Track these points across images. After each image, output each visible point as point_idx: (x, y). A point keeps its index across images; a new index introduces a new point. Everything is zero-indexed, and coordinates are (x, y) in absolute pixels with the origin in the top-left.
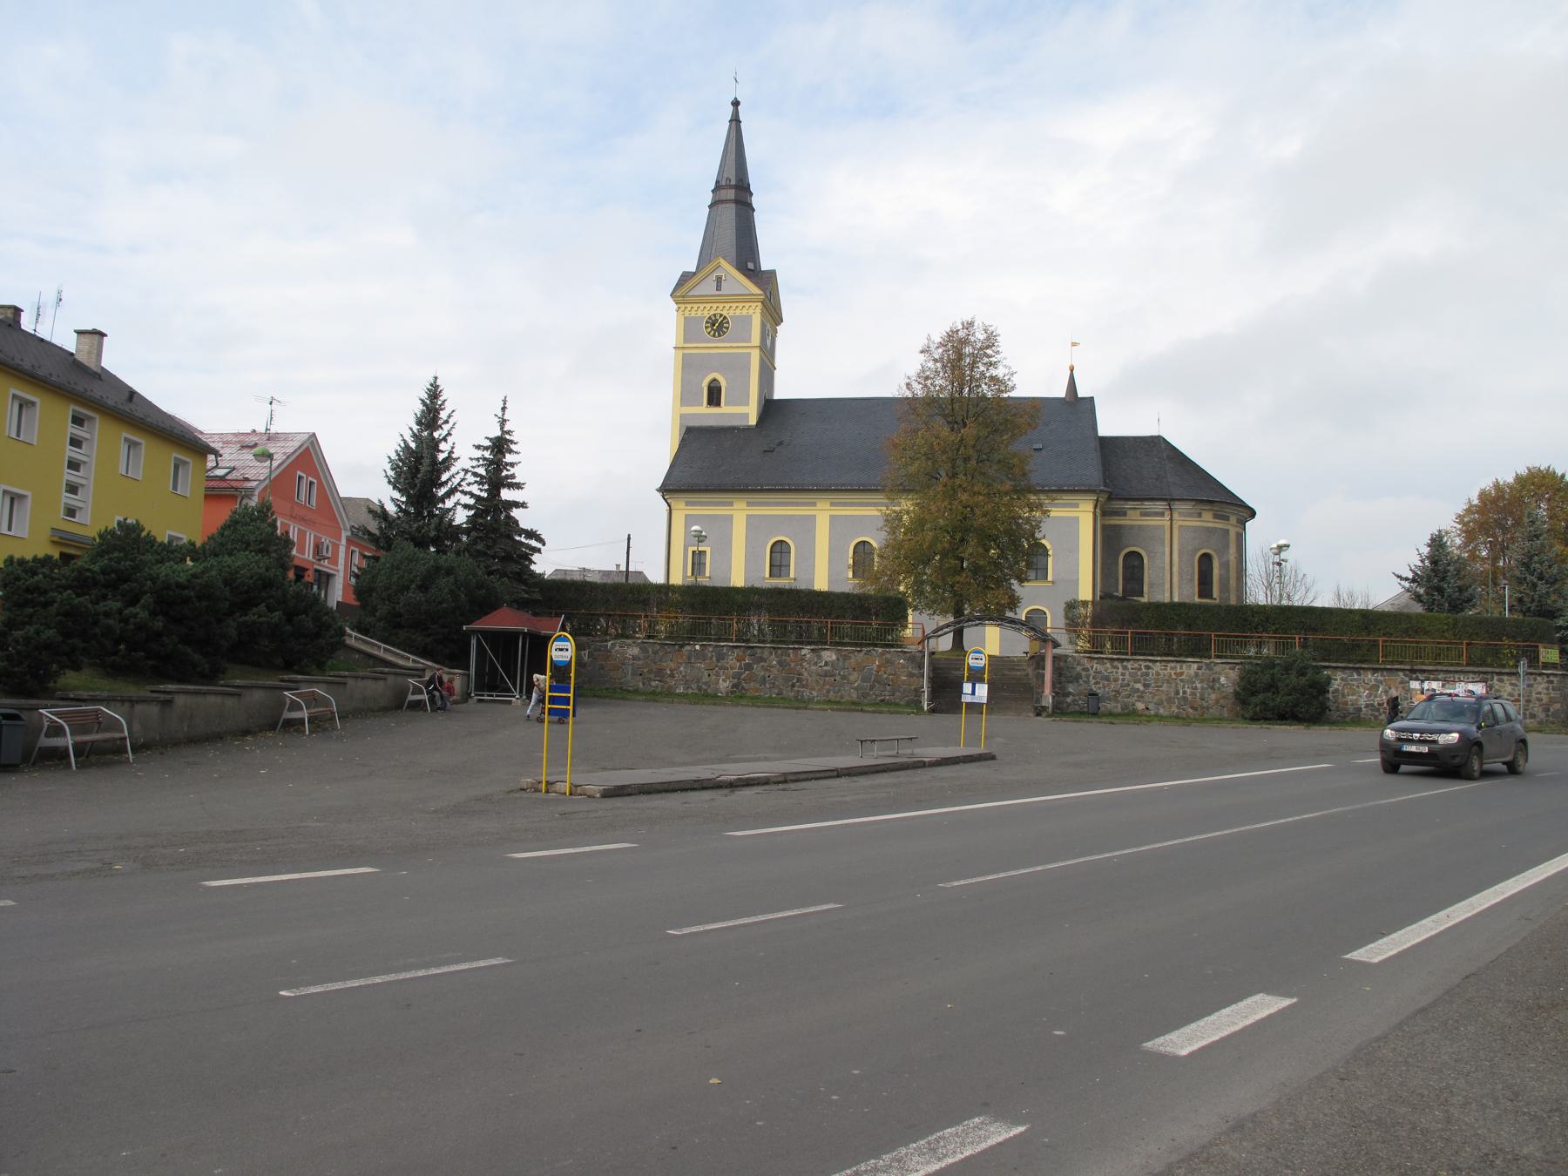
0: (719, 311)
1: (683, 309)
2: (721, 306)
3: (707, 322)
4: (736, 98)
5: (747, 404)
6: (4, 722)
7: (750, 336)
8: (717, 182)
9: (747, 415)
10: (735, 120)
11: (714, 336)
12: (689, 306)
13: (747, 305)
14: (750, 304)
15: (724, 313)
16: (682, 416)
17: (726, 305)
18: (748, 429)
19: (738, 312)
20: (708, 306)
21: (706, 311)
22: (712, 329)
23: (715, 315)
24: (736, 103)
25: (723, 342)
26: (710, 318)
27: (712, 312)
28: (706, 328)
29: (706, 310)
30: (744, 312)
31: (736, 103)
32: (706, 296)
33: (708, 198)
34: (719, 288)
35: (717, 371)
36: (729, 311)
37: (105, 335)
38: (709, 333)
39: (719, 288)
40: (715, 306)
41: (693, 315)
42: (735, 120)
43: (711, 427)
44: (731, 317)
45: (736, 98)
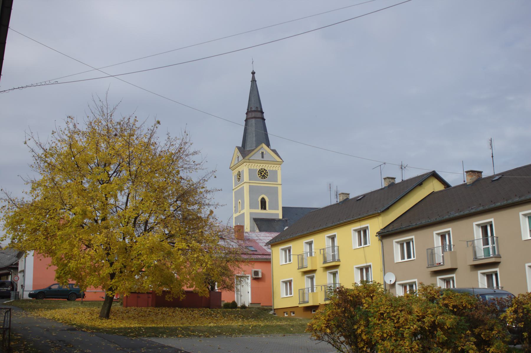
0: (263, 167)
1: (248, 165)
2: (264, 165)
3: (259, 172)
4: (253, 71)
5: (278, 209)
6: (452, 250)
7: (277, 179)
8: (248, 109)
9: (278, 214)
10: (254, 81)
11: (262, 178)
12: (251, 164)
13: (275, 166)
14: (277, 165)
15: (266, 168)
16: (250, 213)
17: (255, 164)
18: (280, 220)
19: (271, 169)
20: (259, 165)
21: (258, 167)
22: (261, 175)
23: (262, 169)
24: (253, 73)
25: (266, 181)
26: (260, 170)
27: (261, 168)
28: (259, 174)
29: (277, 167)
30: (274, 169)
31: (253, 73)
32: (268, 161)
33: (244, 117)
34: (263, 157)
35: (265, 194)
36: (268, 167)
37: (482, 172)
38: (260, 177)
39: (263, 157)
40: (262, 165)
41: (252, 168)
42: (254, 81)
43: (263, 219)
44: (268, 170)
45: (253, 71)
